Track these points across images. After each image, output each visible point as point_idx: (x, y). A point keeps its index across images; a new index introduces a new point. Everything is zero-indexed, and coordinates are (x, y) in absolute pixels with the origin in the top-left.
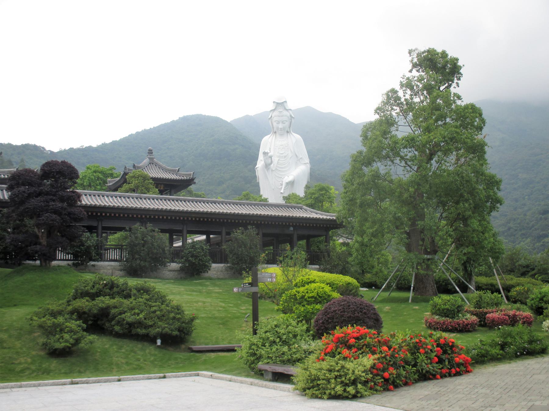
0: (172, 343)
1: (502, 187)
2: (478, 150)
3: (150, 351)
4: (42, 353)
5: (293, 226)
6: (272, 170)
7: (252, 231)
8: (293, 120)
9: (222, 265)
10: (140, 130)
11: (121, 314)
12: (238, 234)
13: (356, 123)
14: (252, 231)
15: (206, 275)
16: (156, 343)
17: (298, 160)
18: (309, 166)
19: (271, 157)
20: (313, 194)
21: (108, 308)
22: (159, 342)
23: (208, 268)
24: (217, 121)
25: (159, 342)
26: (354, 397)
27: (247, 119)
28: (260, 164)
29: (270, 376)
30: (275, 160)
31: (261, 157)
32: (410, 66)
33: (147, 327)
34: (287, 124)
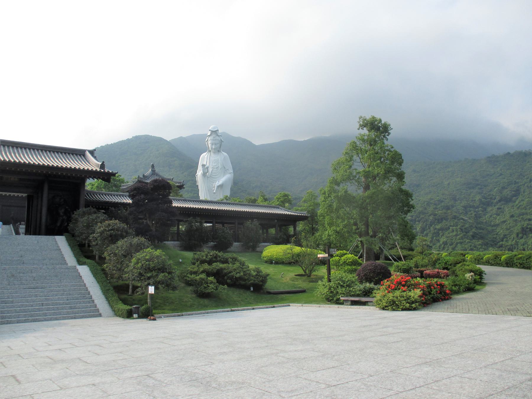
0: (256, 291)
1: (413, 198)
2: (400, 176)
3: (247, 295)
4: (194, 296)
5: (277, 219)
6: (208, 177)
7: (256, 222)
8: (222, 143)
9: (239, 243)
10: (104, 145)
11: (230, 273)
12: (248, 223)
13: (257, 144)
14: (256, 222)
15: (229, 250)
16: (250, 289)
17: (224, 170)
18: (232, 174)
19: (207, 168)
20: (279, 198)
21: (222, 269)
22: (252, 289)
23: (231, 244)
24: (160, 140)
25: (252, 289)
26: (415, 309)
27: (181, 139)
28: (200, 172)
29: (349, 303)
30: (210, 170)
31: (200, 168)
32: (358, 127)
33: (245, 280)
34: (218, 145)
